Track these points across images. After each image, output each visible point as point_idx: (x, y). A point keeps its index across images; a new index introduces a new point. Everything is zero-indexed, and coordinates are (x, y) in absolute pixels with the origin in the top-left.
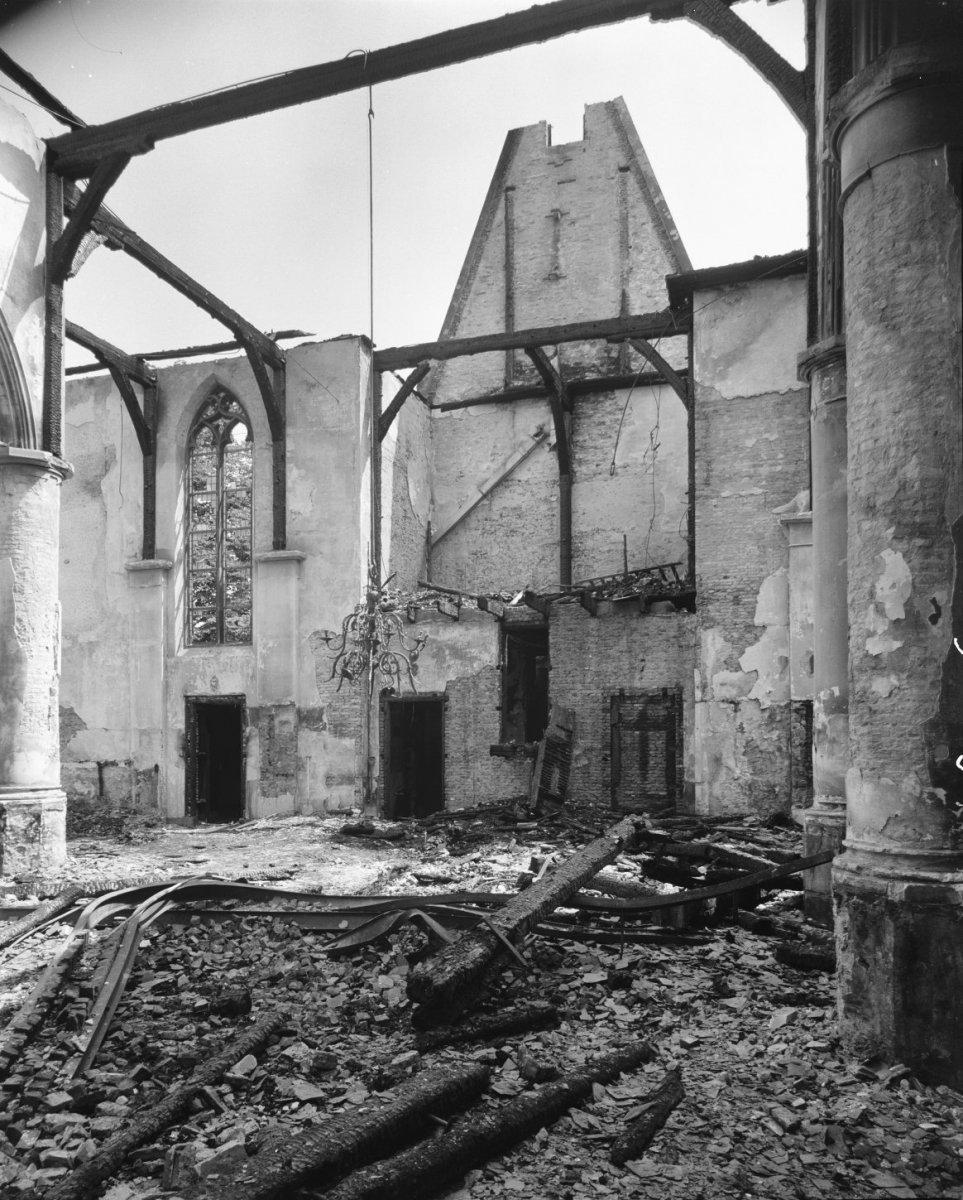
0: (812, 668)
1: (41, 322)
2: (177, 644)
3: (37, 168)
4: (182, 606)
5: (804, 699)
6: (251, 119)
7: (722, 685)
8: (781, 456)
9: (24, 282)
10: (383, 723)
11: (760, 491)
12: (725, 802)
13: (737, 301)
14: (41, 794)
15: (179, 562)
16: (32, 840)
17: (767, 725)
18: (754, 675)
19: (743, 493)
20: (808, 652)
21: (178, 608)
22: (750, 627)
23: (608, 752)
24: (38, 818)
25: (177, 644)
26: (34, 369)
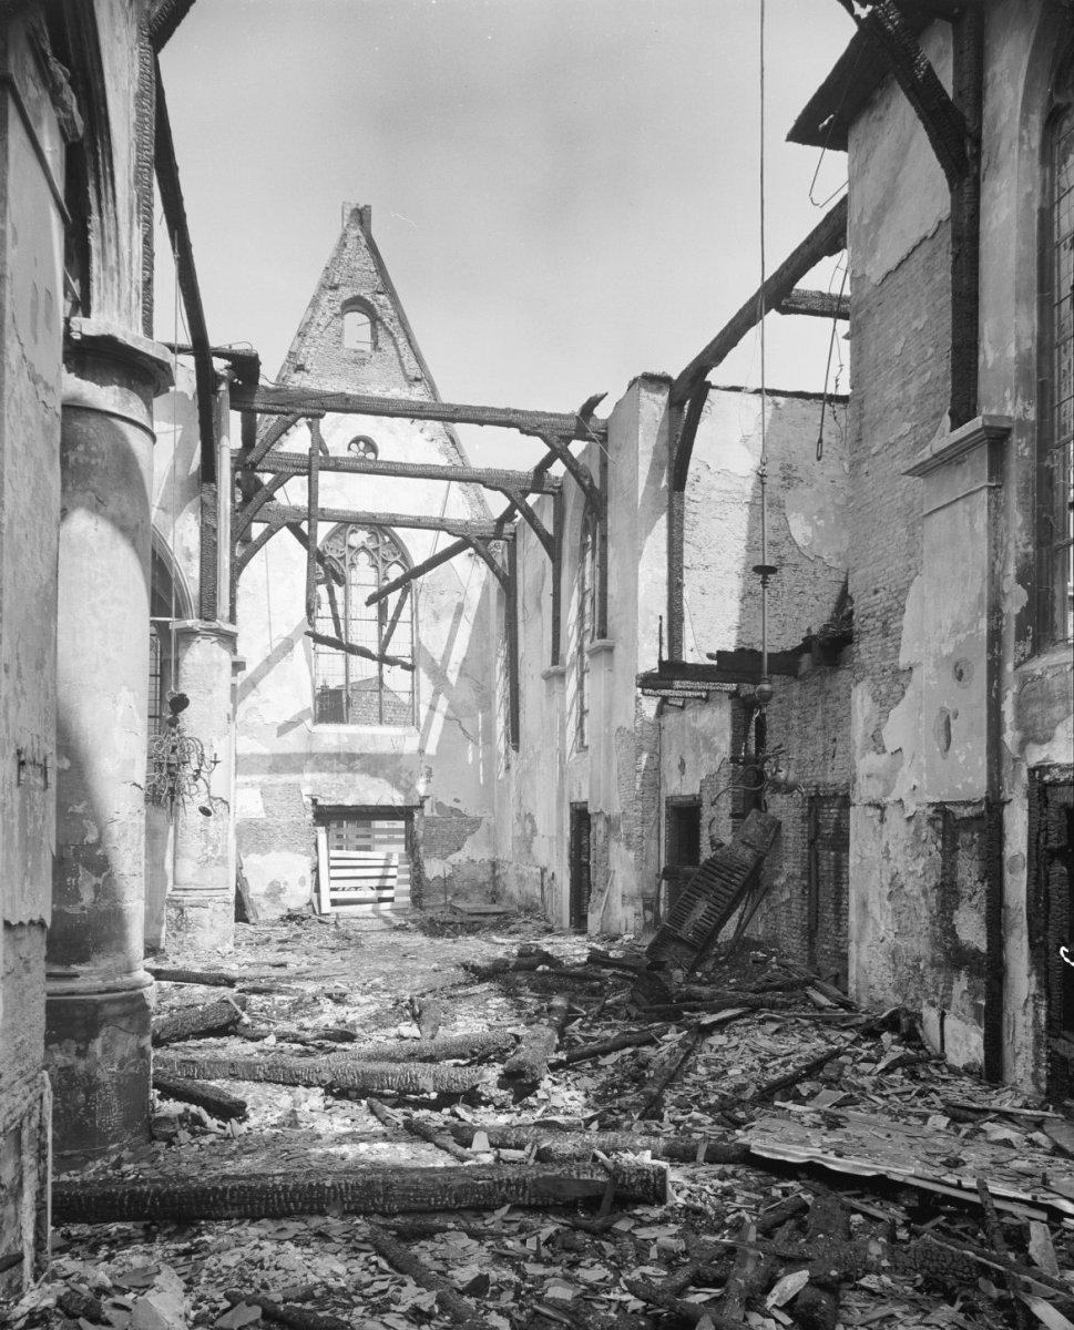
0: (948, 746)
1: (196, 518)
2: (569, 749)
3: (191, 397)
4: (574, 711)
5: (937, 800)
6: (814, 90)
7: (868, 776)
8: (931, 351)
9: (178, 492)
10: (670, 832)
11: (907, 426)
12: (873, 980)
13: (888, 107)
14: (190, 893)
15: (572, 665)
16: (179, 929)
17: (912, 846)
18: (880, 749)
19: (891, 440)
20: (943, 710)
21: (571, 713)
22: (897, 672)
23: (805, 882)
24: (182, 911)
25: (569, 749)
26: (189, 557)
